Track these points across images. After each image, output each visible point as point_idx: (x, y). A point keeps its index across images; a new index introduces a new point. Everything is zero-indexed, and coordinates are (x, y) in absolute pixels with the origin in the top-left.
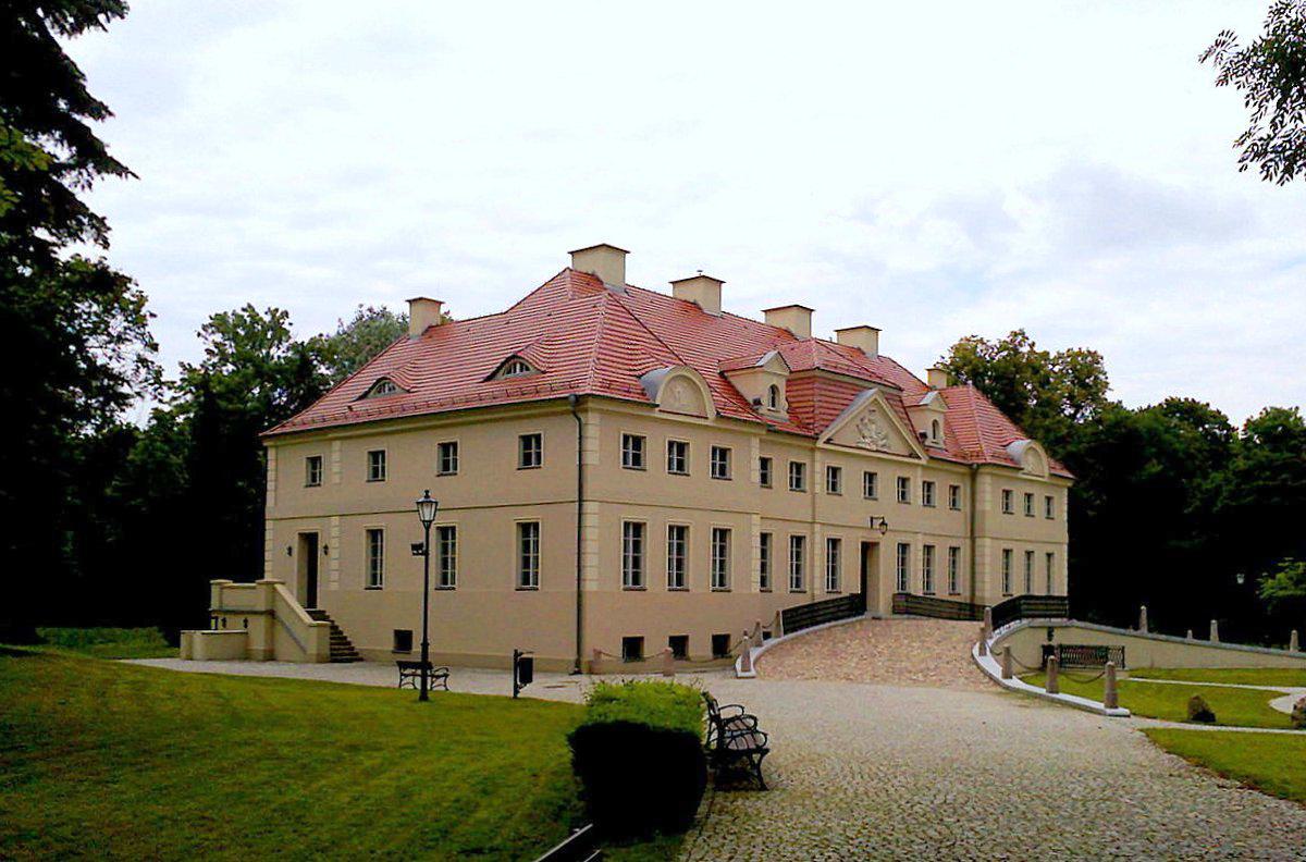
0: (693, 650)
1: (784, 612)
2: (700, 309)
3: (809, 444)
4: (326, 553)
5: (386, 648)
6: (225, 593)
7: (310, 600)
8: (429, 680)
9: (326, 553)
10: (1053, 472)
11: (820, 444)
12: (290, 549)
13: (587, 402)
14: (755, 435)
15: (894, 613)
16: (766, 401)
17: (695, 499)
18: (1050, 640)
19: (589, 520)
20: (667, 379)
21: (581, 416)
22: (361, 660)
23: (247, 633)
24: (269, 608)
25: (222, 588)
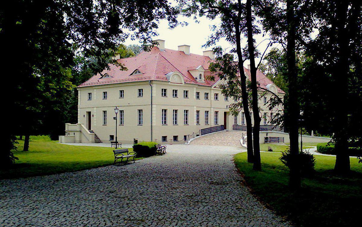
0: (179, 139)
1: (201, 130)
2: (184, 53)
3: (210, 88)
4: (93, 116)
5: (108, 139)
6: (69, 127)
7: (90, 128)
8: (117, 145)
9: (93, 116)
10: (279, 92)
11: (212, 88)
12: (84, 115)
13: (153, 82)
14: (195, 87)
15: (233, 130)
16: (198, 78)
17: (179, 103)
18: (267, 136)
19: (153, 109)
20: (173, 75)
21: (151, 85)
22: (102, 142)
23: (74, 136)
24: (80, 130)
25: (68, 125)
